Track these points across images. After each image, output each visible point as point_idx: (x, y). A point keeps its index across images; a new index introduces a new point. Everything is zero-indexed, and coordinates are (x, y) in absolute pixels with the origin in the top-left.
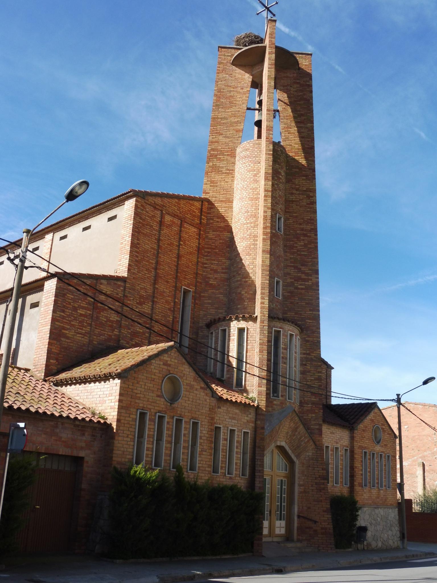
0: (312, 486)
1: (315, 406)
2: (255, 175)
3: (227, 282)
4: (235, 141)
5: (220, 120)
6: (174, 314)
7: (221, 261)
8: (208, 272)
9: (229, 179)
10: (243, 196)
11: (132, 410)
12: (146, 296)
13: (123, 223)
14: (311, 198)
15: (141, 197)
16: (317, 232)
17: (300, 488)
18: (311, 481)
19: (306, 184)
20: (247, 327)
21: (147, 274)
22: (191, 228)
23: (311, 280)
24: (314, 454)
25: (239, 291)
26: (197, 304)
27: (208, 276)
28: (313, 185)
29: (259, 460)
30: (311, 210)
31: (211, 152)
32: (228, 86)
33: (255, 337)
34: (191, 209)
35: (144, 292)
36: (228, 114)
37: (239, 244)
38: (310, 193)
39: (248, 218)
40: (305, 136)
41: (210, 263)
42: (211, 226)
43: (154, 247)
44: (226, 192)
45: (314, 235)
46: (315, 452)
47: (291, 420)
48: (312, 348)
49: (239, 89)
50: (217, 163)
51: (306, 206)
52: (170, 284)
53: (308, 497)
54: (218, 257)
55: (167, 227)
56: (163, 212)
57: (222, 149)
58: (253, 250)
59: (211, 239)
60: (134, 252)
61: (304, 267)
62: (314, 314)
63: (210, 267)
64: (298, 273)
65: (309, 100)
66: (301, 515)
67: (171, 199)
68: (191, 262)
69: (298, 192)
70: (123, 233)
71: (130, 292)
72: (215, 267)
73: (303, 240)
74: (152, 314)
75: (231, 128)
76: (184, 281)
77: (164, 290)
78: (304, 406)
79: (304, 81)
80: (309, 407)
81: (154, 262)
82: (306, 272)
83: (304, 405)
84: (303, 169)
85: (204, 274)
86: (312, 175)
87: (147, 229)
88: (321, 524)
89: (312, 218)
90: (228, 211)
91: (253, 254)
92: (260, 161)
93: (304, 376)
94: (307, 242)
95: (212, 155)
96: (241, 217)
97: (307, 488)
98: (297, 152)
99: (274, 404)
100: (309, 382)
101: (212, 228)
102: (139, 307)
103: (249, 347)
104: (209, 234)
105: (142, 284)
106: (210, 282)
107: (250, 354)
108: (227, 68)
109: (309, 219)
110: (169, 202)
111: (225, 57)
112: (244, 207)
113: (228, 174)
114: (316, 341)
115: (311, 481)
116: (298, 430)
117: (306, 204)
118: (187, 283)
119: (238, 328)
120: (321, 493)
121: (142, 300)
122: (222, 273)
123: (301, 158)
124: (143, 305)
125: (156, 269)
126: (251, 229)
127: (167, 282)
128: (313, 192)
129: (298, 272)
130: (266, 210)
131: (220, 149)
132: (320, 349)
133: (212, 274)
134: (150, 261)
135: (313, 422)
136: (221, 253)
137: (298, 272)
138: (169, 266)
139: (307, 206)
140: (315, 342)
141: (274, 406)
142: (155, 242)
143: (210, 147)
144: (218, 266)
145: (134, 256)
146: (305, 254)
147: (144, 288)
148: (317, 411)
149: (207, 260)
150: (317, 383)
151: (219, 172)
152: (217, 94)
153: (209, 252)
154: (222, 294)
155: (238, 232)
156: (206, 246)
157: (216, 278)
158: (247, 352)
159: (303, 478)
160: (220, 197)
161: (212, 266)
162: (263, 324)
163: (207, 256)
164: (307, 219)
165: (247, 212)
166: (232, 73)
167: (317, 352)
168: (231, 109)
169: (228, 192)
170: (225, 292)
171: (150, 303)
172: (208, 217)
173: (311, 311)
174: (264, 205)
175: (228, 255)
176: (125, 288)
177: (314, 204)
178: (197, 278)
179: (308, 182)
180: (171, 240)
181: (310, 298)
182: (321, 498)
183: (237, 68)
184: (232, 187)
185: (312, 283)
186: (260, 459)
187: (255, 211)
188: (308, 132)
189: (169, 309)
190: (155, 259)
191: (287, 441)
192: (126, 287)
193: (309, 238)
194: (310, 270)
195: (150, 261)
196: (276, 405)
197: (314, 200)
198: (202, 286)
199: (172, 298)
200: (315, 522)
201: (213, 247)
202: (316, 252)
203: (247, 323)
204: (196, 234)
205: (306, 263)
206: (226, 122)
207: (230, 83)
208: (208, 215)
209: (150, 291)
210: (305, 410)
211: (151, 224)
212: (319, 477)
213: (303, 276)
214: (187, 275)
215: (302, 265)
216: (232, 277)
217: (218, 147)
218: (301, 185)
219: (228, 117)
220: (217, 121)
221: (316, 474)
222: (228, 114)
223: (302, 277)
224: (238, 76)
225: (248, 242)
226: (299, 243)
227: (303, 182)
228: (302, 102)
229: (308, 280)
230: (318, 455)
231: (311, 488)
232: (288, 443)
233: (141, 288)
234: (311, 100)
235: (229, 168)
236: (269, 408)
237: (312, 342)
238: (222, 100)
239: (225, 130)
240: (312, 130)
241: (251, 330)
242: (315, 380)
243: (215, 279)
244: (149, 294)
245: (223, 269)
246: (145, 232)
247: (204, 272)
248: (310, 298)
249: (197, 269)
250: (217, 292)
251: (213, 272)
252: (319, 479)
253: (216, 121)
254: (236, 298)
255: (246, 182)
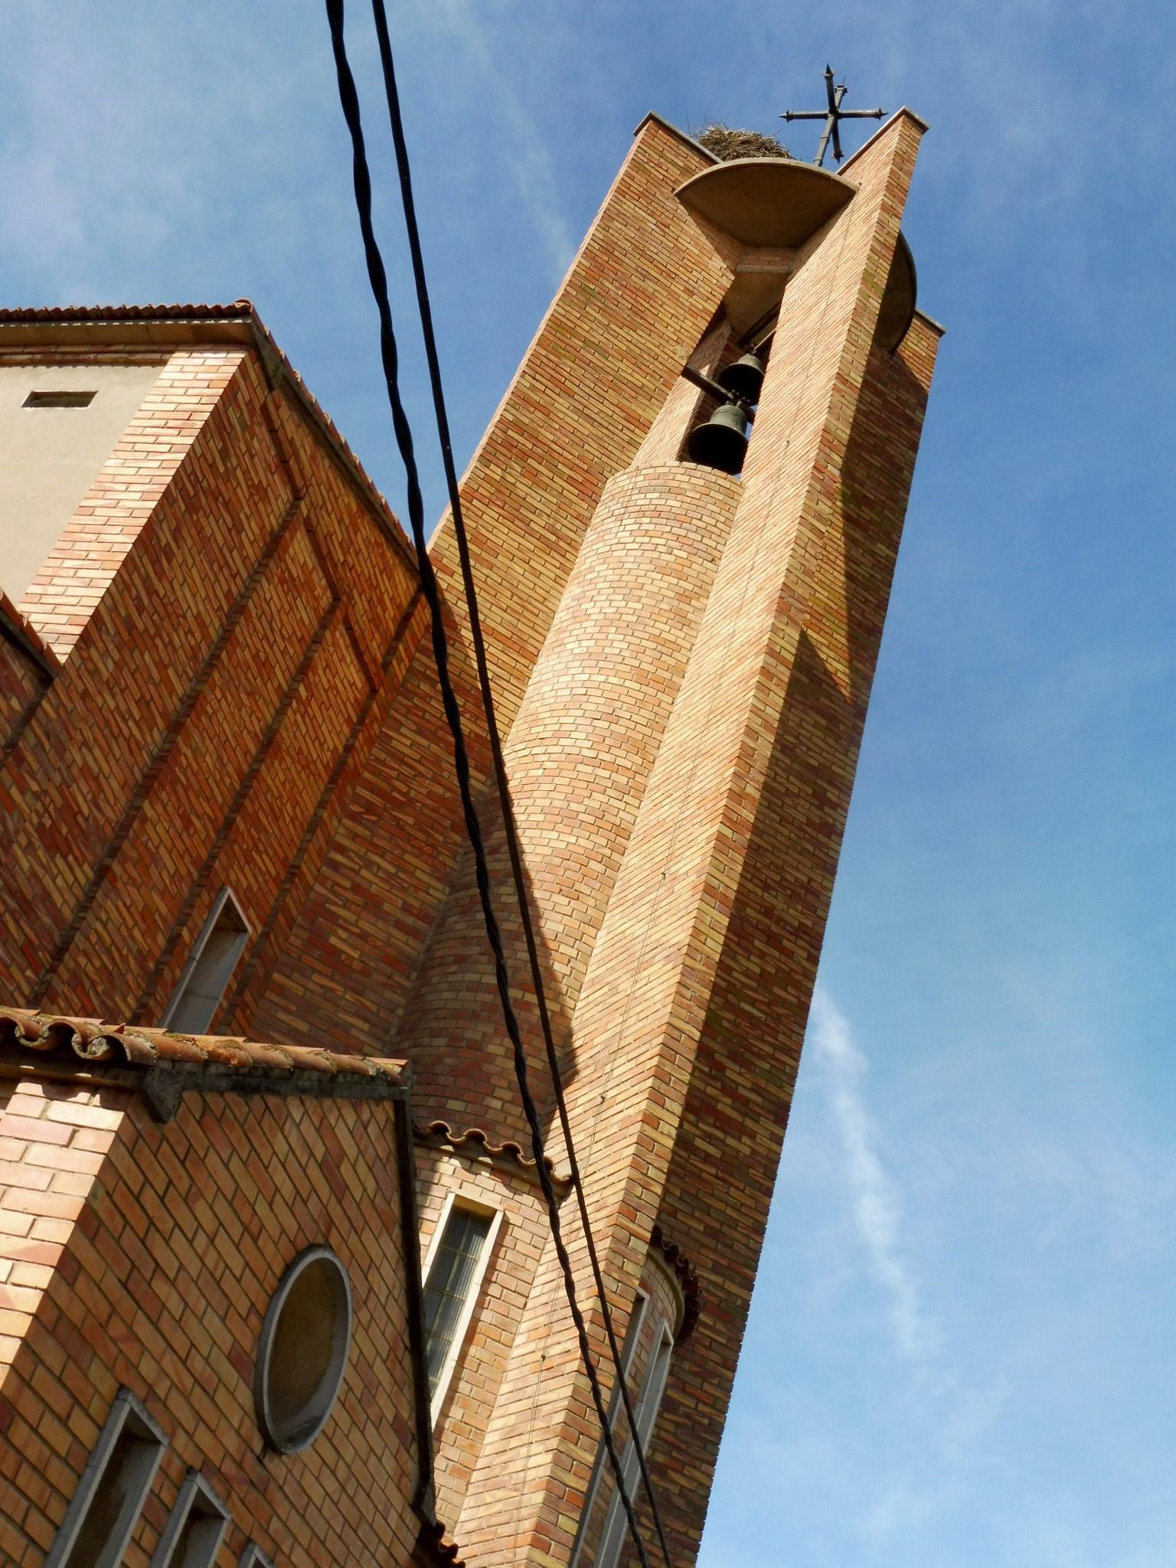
2: (684, 597)
3: (408, 977)
4: (610, 448)
5: (581, 344)
6: (150, 994)
7: (411, 874)
8: (340, 891)
9: (547, 565)
10: (607, 650)
11: (96, 1370)
12: (86, 819)
13: (128, 430)
14: (827, 809)
15: (264, 368)
16: (819, 948)
19: (824, 746)
20: (505, 1215)
21: (134, 720)
22: (348, 660)
23: (752, 1135)
25: (473, 1034)
26: (245, 1006)
27: (334, 909)
28: (846, 764)
30: (817, 852)
31: (510, 432)
32: (643, 253)
33: (527, 1277)
34: (378, 584)
35: (89, 797)
36: (615, 341)
37: (528, 833)
38: (829, 788)
39: (608, 741)
40: (860, 577)
41: (361, 858)
42: (417, 707)
43: (208, 621)
44: (520, 609)
45: (805, 955)
48: (684, 1447)
49: (678, 288)
50: (518, 484)
51: (800, 829)
52: (190, 837)
54: (404, 851)
55: (282, 581)
56: (303, 505)
57: (554, 446)
58: (597, 885)
59: (401, 759)
60: (140, 575)
61: (737, 1069)
62: (729, 1293)
63: (357, 872)
64: (708, 1084)
65: (900, 469)
67: (339, 481)
68: (295, 804)
69: (787, 761)
70: (111, 471)
71: (43, 747)
72: (377, 886)
73: (762, 955)
74: (74, 929)
75: (611, 395)
76: (241, 869)
77: (163, 851)
79: (898, 399)
81: (180, 691)
82: (741, 1090)
84: (824, 686)
85: (318, 887)
86: (851, 725)
87: (217, 522)
89: (813, 884)
90: (504, 684)
91: (592, 902)
92: (718, 554)
94: (773, 971)
95: (509, 445)
96: (573, 727)
98: (820, 617)
101: (417, 716)
102: (41, 853)
103: (486, 1316)
104: (397, 731)
105: (97, 752)
106: (333, 940)
107: (485, 1356)
108: (658, 195)
109: (802, 886)
110: (331, 489)
111: (662, 160)
112: (599, 693)
113: (550, 547)
114: (706, 1421)
117: (801, 818)
118: (245, 885)
119: (457, 1196)
121: (65, 830)
122: (399, 925)
123: (826, 643)
124: (59, 860)
125: (176, 727)
126: (609, 792)
127: (187, 824)
128: (841, 790)
129: (709, 1075)
130: (757, 728)
131: (550, 443)
132: (713, 1463)
133: (353, 907)
134: (170, 671)
136: (422, 837)
137: (709, 1075)
138: (220, 758)
139: (806, 828)
140: (700, 1424)
142: (221, 607)
143: (513, 411)
144: (393, 886)
145: (130, 593)
146: (754, 1017)
147: (96, 779)
149: (354, 837)
151: (517, 522)
152: (598, 253)
153: (370, 809)
154: (366, 1020)
155: (537, 782)
156: (366, 775)
157: (364, 936)
158: (469, 1339)
160: (491, 615)
161: (364, 873)
162: (631, 1225)
163: (353, 817)
164: (796, 879)
165: (613, 717)
166: (670, 222)
167: (697, 1474)
168: (631, 332)
169: (526, 613)
170: (382, 1014)
171: (86, 867)
172: (416, 665)
173: (717, 1273)
174: (754, 706)
175: (449, 862)
176: (31, 711)
177: (833, 837)
178: (288, 891)
179: (832, 743)
180: (271, 647)
181: (729, 1211)
183: (689, 218)
184: (548, 604)
185: (754, 1152)
187: (648, 731)
188: (872, 568)
189: (142, 958)
190: (190, 680)
192: (39, 713)
193: (783, 958)
194: (756, 1089)
195: (170, 671)
197: (837, 823)
198: (292, 939)
199: (170, 910)
201: (395, 794)
202: (796, 1028)
203: (511, 1195)
204: (356, 699)
205: (747, 1055)
206: (601, 365)
207: (652, 248)
208: (417, 655)
209: (113, 814)
211: (242, 516)
213: (725, 1105)
214: (261, 848)
215: (733, 1056)
216: (451, 959)
217: (542, 431)
218: (806, 741)
219: (612, 352)
220: (566, 340)
222: (615, 341)
223: (720, 1107)
224: (685, 242)
225: (582, 842)
226: (743, 961)
227: (812, 734)
228: (876, 461)
229: (742, 1131)
233: (85, 770)
234: (906, 473)
235: (558, 526)
237: (687, 1416)
238: (607, 283)
239: (587, 390)
240: (888, 568)
241: (517, 1233)
243: (357, 935)
244: (102, 821)
245: (406, 908)
246: (209, 532)
247: (323, 885)
248: (729, 1211)
249: (301, 850)
250: (347, 997)
251: (360, 900)
253: (562, 338)
254: (448, 1060)
255: (639, 606)
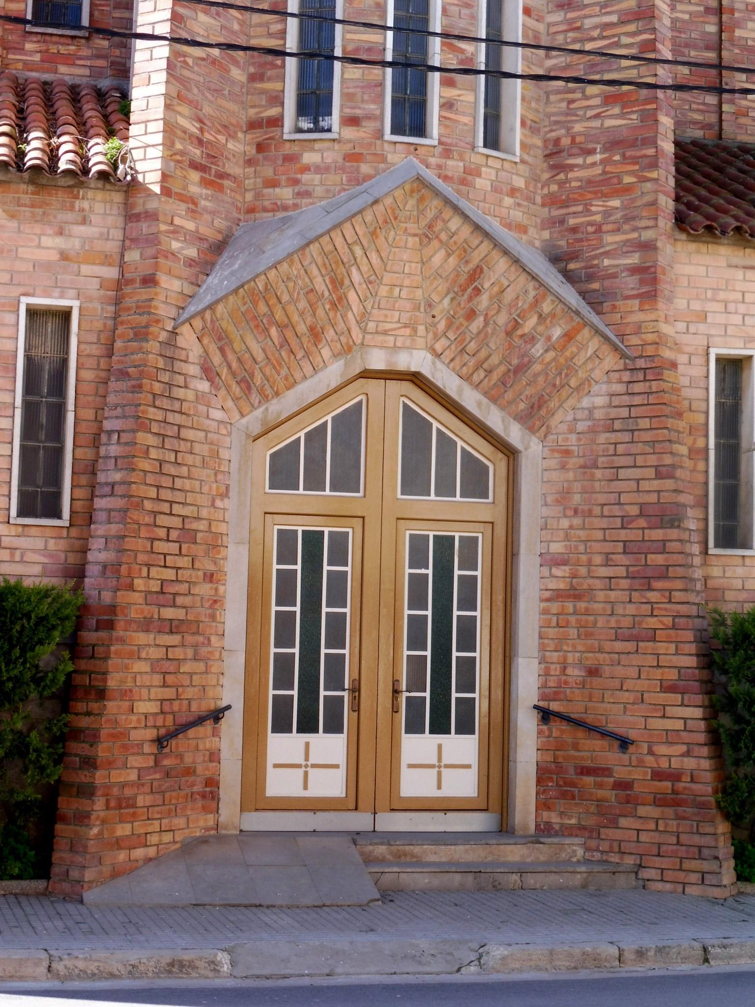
0: (607, 562)
1: (624, 156)
17: (552, 576)
18: (599, 535)
24: (616, 401)
29: (116, 436)
46: (620, 388)
47: (427, 236)
53: (591, 618)
66: (555, 706)
78: (571, 167)
80: (594, 164)
83: (571, 161)
88: (651, 752)
93: (570, 15)
97: (583, 571)
99: (306, 169)
100: (593, 39)
115: (599, 535)
116: (487, 285)
120: (653, 596)
135: (611, 240)
141: (305, 177)
148: (634, 180)
150: (627, 34)
159: (565, 523)
182: (652, 622)
186: (119, 432)
191: (439, 347)
196: (319, 169)
200: (624, 743)
210: (574, 184)
212: (641, 514)
221: (624, 498)
230: (637, 400)
231: (604, 572)
232: (448, 355)
236: (277, 190)
242: (622, 23)
252: (642, 523)
